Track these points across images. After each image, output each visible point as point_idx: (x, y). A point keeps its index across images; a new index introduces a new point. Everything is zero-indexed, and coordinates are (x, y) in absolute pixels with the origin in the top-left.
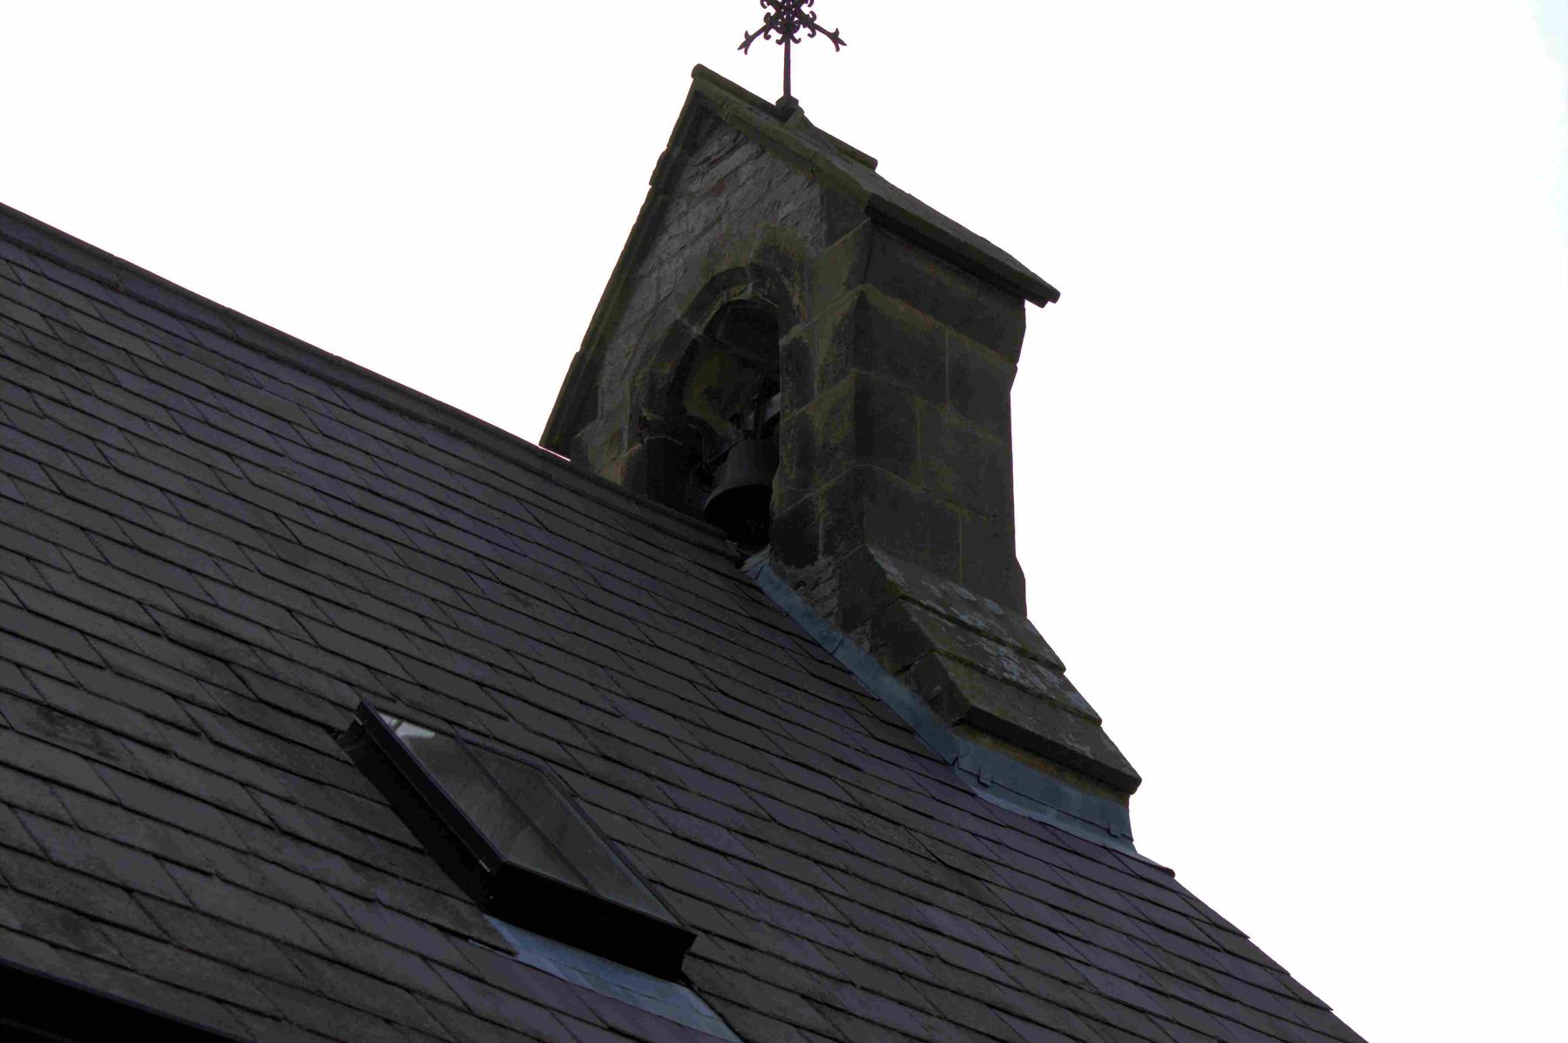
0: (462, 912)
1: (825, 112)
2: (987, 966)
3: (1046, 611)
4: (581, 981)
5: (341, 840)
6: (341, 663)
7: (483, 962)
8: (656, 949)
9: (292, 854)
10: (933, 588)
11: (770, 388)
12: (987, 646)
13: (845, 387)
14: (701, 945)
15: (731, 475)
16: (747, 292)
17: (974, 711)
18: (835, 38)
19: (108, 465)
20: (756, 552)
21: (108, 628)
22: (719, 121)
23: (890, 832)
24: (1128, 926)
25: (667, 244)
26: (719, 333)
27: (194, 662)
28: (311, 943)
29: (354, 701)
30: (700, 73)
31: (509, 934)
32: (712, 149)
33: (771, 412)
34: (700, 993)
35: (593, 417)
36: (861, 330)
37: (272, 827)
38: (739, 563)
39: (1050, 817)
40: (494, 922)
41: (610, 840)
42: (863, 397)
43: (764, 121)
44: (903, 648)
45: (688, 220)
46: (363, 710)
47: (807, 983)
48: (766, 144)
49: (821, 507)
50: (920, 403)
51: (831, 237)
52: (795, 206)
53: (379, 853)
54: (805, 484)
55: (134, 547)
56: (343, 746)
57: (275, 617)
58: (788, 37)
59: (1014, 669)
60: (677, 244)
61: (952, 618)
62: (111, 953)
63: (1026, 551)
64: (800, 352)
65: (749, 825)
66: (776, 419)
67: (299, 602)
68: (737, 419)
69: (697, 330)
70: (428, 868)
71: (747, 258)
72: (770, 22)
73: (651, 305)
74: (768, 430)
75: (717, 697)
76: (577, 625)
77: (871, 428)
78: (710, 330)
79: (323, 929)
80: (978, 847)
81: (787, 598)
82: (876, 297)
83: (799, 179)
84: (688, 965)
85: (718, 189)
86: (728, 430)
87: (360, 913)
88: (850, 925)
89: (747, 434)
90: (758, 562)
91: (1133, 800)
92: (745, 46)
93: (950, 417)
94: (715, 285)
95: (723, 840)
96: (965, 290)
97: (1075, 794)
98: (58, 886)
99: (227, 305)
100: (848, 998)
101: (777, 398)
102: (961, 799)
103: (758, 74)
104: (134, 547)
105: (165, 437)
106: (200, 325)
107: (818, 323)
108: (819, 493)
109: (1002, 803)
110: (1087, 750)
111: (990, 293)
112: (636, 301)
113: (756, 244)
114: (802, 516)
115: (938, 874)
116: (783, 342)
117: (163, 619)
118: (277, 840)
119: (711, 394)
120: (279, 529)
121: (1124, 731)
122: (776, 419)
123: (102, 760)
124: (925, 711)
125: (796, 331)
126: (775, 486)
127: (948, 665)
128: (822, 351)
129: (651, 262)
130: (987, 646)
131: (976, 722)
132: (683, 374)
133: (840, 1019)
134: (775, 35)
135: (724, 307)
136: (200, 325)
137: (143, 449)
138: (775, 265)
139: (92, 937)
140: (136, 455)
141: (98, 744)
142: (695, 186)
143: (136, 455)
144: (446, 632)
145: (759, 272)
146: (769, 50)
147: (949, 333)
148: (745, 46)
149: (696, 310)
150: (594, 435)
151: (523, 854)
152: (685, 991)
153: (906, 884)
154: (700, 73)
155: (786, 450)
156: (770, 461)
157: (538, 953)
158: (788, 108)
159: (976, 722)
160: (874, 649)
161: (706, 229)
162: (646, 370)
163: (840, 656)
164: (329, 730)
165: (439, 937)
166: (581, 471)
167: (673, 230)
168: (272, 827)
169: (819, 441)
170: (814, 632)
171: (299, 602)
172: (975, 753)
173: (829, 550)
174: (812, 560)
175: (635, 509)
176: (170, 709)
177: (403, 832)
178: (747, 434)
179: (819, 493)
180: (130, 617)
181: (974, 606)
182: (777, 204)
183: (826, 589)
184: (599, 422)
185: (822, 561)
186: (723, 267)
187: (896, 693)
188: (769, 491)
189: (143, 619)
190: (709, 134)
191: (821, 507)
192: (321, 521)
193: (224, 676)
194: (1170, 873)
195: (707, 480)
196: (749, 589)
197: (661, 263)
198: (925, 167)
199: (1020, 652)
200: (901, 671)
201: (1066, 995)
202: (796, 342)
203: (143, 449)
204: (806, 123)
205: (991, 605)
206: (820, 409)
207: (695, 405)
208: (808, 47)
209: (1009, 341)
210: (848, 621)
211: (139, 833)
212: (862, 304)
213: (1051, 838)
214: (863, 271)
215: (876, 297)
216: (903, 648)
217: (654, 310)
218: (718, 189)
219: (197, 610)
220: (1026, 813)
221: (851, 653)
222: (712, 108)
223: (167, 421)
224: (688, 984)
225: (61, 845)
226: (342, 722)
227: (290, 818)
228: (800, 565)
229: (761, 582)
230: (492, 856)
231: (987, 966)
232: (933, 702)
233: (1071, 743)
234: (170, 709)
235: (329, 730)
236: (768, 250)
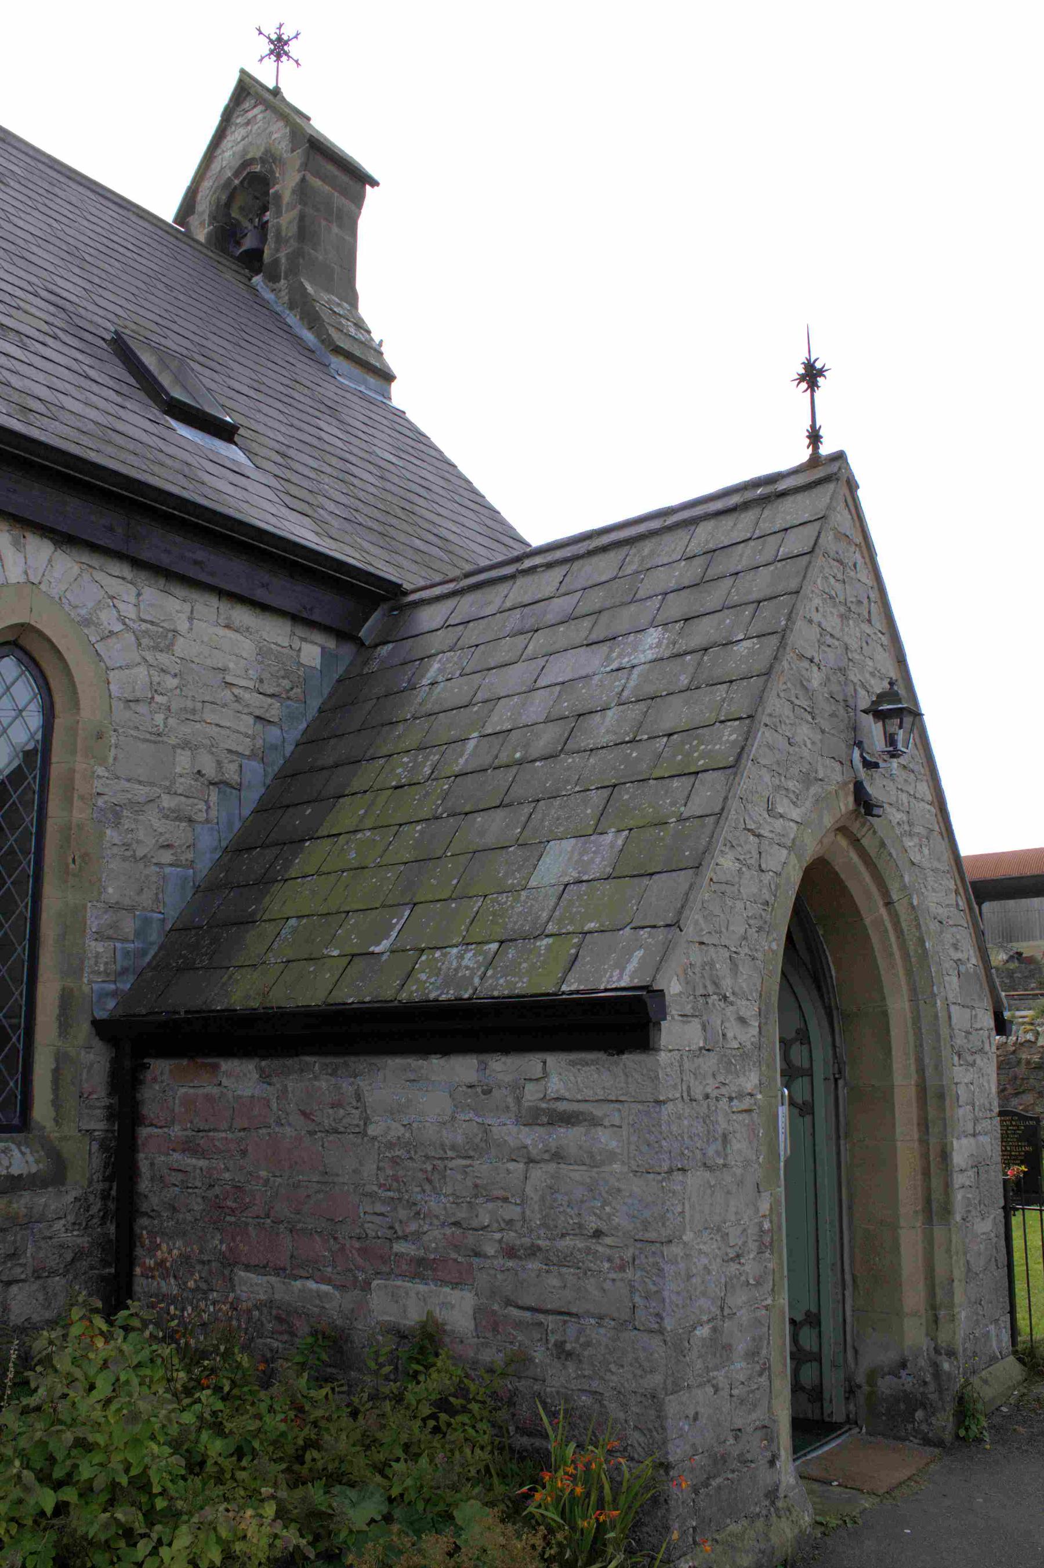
0: (155, 413)
1: (293, 95)
2: (340, 444)
3: (368, 309)
4: (199, 442)
5: (111, 383)
6: (105, 312)
7: (166, 433)
8: (226, 432)
9: (95, 388)
10: (325, 296)
11: (265, 209)
12: (344, 321)
13: (295, 213)
14: (241, 431)
15: (248, 243)
16: (258, 168)
17: (338, 346)
18: (297, 62)
19: (10, 222)
20: (257, 274)
21: (19, 293)
22: (249, 93)
23: (306, 391)
24: (389, 432)
25: (227, 143)
26: (246, 184)
27: (52, 309)
28: (105, 423)
29: (113, 329)
30: (243, 72)
31: (174, 423)
32: (247, 105)
33: (265, 219)
34: (240, 448)
35: (193, 213)
36: (303, 190)
37: (87, 377)
38: (250, 280)
39: (362, 389)
40: (168, 418)
41: (208, 389)
42: (302, 218)
43: (267, 96)
44: (313, 320)
45: (236, 135)
46: (116, 332)
47: (277, 446)
48: (268, 107)
49: (283, 260)
50: (324, 223)
51: (293, 151)
52: (279, 133)
53: (125, 389)
54: (277, 250)
55: (23, 258)
56: (109, 345)
57: (78, 291)
58: (278, 57)
59: (352, 331)
60: (230, 145)
61: (331, 309)
62: (38, 424)
63: (360, 285)
64: (278, 196)
65: (256, 385)
66: (267, 222)
67: (88, 286)
68: (251, 221)
69: (237, 182)
70: (142, 396)
71: (258, 155)
72: (272, 52)
73: (218, 169)
74: (264, 226)
75: (243, 334)
76: (190, 301)
77: (305, 232)
78: (242, 182)
79: (110, 418)
80: (336, 398)
81: (269, 296)
82: (309, 177)
83: (281, 124)
84: (236, 438)
85: (248, 123)
86: (246, 224)
87: (122, 413)
88: (292, 426)
89: (255, 227)
90: (257, 280)
91: (393, 384)
92: (261, 60)
93: (335, 229)
94: (246, 164)
95: (245, 390)
96: (344, 178)
97: (372, 380)
98: (16, 397)
99: (954, 827)
100: (291, 453)
101: (268, 214)
102: (332, 380)
103: (265, 74)
104: (23, 258)
105: (29, 210)
106: (39, 161)
107: (286, 184)
108: (282, 256)
109: (346, 382)
110: (378, 364)
111: (355, 180)
112: (213, 166)
113: (262, 149)
114: (276, 262)
115: (323, 408)
116: (272, 191)
117: (39, 290)
118: (90, 383)
119: (242, 209)
120: (77, 254)
121: (392, 358)
122: (267, 222)
123: (24, 348)
124: (319, 344)
125: (277, 187)
126: (266, 251)
127: (328, 327)
128: (287, 197)
129: (219, 151)
130: (344, 321)
131: (338, 351)
132: (231, 198)
133: (289, 461)
134: (273, 58)
135: (248, 173)
136: (39, 161)
137: (23, 215)
138: (269, 158)
139: (31, 417)
140: (20, 218)
141: (21, 341)
142: (238, 121)
143: (20, 218)
144: (142, 301)
145: (263, 161)
146: (270, 62)
147: (336, 194)
148: (261, 60)
149: (236, 174)
150: (194, 221)
151: (177, 393)
152: (234, 447)
153: (311, 411)
154: (243, 72)
155: (271, 236)
156: (263, 239)
157: (183, 430)
158: (276, 92)
159: (338, 351)
160: (301, 319)
161: (243, 139)
162: (215, 196)
163: (288, 320)
164: (103, 339)
165: (149, 423)
166: (188, 235)
167: (229, 138)
168: (87, 377)
169: (283, 234)
170: (278, 309)
171: (88, 286)
172: (337, 362)
173: (286, 278)
174: (279, 281)
175: (210, 254)
176: (45, 328)
177: (132, 381)
178: (255, 227)
179: (282, 256)
180: (26, 288)
181: (339, 305)
182: (271, 133)
183: (283, 293)
184: (196, 216)
185: (282, 281)
186: (249, 157)
187: (309, 336)
188: (263, 252)
189: (30, 289)
190: (245, 99)
191: (283, 260)
192: (92, 251)
193: (63, 315)
194: (404, 413)
195: (238, 244)
196: (253, 289)
197: (223, 152)
198: (332, 126)
199: (355, 324)
200: (310, 329)
201: (366, 456)
202: (277, 192)
203: (23, 215)
204: (284, 100)
205: (345, 305)
206: (284, 220)
207: (235, 214)
208: (286, 64)
209: (358, 200)
210: (292, 306)
211: (40, 377)
212: (303, 180)
213: (363, 397)
214: (305, 166)
215: (309, 177)
216: (313, 320)
217: (220, 172)
218: (248, 123)
219: (51, 287)
220: (353, 386)
221: (292, 319)
222: (246, 90)
223: (30, 203)
224: (236, 445)
225: (15, 381)
226: (108, 337)
227: (92, 373)
228: (274, 283)
229: (258, 288)
230: (167, 394)
231: (340, 444)
232: (323, 342)
233: (373, 361)
234: (45, 328)
235: (103, 339)
236: (267, 151)
